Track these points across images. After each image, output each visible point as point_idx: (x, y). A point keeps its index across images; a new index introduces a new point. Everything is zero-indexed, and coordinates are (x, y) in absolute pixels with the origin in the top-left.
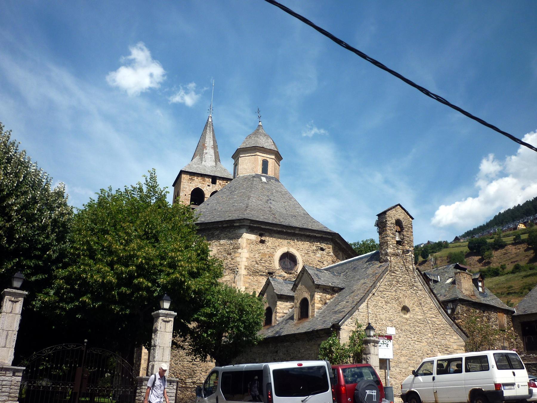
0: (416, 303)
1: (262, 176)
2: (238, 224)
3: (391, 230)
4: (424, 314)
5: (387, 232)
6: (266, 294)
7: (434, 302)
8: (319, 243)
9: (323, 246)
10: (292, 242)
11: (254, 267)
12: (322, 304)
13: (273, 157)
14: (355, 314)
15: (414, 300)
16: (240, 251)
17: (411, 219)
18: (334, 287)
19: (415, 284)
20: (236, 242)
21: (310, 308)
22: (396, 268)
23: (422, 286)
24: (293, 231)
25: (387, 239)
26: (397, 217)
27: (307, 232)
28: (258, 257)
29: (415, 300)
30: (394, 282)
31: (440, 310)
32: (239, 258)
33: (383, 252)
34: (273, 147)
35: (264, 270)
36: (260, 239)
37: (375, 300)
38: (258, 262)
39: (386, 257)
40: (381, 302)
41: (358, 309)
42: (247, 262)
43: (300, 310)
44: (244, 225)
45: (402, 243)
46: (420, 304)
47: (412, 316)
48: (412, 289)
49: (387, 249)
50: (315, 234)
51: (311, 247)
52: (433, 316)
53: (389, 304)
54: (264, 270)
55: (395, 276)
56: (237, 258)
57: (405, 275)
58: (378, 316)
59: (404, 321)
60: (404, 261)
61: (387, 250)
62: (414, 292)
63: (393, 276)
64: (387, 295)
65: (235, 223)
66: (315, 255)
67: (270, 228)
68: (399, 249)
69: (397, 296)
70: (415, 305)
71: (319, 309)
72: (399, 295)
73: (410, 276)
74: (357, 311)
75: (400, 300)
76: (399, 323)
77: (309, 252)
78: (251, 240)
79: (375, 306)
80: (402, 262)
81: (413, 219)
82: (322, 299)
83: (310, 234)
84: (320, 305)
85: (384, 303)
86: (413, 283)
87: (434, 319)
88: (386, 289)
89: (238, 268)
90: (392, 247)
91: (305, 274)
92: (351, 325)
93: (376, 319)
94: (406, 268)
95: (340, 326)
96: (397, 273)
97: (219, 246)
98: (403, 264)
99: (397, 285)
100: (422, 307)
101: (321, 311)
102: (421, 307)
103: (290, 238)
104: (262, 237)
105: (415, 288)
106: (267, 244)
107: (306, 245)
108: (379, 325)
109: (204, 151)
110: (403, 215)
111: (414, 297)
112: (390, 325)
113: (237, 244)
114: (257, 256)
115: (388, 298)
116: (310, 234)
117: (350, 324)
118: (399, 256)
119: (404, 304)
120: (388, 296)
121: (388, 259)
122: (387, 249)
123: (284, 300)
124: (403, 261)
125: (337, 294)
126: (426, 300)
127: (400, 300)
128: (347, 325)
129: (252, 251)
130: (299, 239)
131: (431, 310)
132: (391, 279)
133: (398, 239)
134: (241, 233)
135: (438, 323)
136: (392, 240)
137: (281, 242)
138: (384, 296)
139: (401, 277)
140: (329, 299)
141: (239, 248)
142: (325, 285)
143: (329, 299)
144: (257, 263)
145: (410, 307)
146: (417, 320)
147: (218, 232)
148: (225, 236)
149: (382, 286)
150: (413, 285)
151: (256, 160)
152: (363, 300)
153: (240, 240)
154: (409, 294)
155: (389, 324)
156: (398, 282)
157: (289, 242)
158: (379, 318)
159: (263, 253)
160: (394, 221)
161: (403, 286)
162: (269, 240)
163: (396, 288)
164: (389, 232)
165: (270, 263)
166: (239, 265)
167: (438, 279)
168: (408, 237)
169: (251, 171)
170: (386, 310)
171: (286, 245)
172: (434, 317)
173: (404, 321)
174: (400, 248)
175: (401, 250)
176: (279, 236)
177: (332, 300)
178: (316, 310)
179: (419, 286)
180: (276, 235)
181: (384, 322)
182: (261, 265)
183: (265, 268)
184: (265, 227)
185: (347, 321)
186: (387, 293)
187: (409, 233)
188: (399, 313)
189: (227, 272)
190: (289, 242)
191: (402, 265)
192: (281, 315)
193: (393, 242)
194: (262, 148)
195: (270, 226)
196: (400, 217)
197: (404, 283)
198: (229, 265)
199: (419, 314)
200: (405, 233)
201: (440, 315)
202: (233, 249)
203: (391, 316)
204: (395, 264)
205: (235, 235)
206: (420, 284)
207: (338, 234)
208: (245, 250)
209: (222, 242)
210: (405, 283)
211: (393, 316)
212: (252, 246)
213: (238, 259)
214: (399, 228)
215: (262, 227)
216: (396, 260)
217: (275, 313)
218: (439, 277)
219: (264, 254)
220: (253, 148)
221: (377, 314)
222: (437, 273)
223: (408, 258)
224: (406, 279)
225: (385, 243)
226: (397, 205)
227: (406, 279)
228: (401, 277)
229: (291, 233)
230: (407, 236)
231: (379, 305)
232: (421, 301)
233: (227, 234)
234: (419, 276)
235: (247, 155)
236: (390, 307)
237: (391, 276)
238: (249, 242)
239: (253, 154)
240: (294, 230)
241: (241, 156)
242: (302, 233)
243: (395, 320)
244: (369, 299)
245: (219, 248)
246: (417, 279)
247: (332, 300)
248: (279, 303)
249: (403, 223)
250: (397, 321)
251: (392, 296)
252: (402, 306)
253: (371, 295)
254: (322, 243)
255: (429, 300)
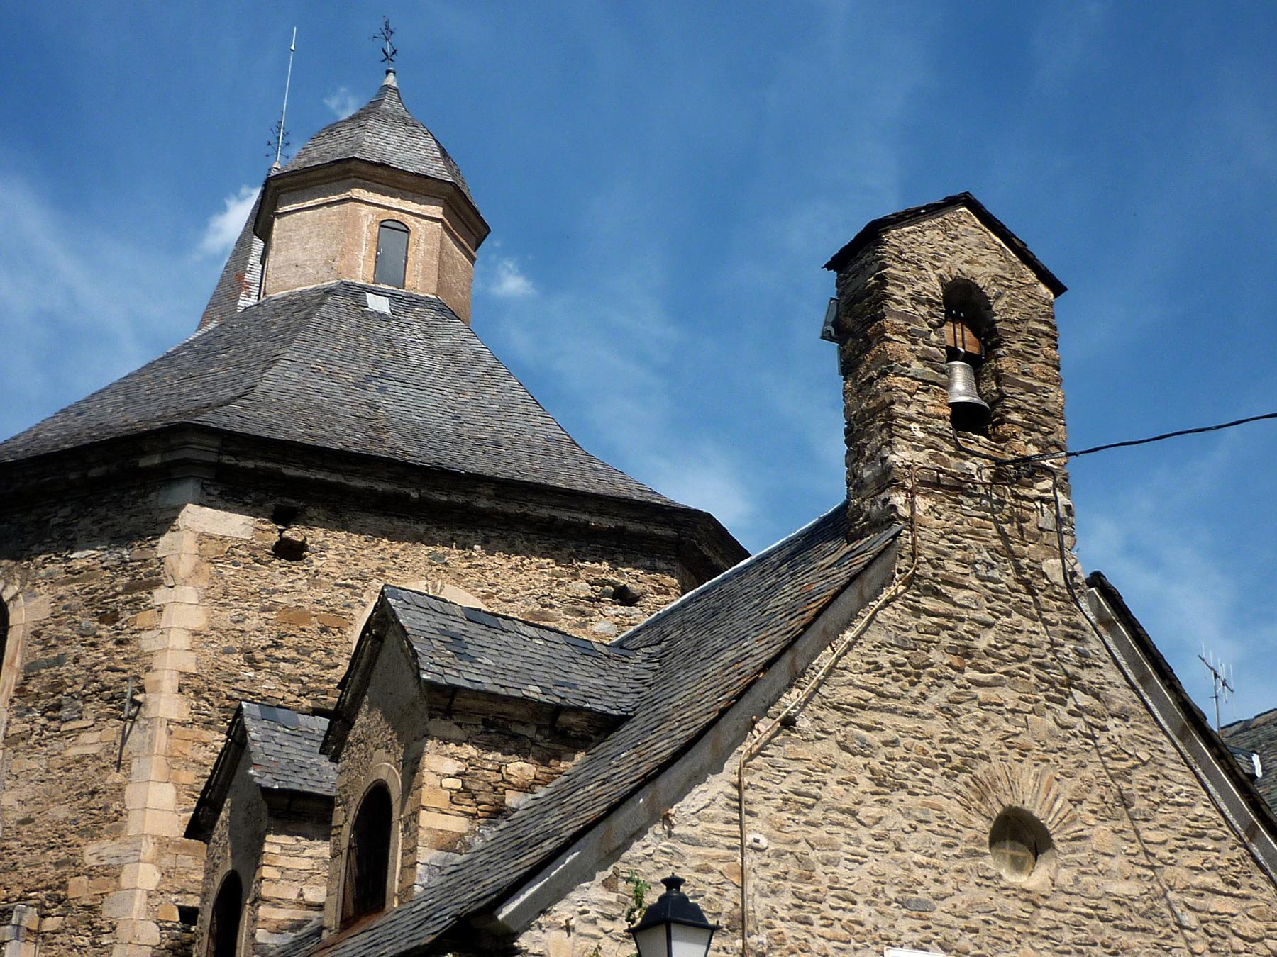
0: (1093, 797)
1: (375, 292)
2: (156, 460)
3: (913, 337)
4: (1152, 868)
5: (890, 346)
6: (228, 803)
7: (1218, 797)
8: (605, 566)
9: (630, 577)
10: (455, 557)
11: (234, 678)
12: (474, 816)
13: (436, 211)
14: (636, 850)
15: (1082, 773)
16: (159, 595)
17: (1043, 290)
18: (558, 710)
19: (1086, 675)
20: (148, 554)
21: (398, 840)
22: (950, 565)
23: (1133, 688)
24: (458, 498)
25: (889, 389)
26: (955, 265)
27: (541, 505)
28: (261, 631)
29: (1087, 774)
30: (935, 656)
31: (1255, 848)
32: (156, 633)
33: (867, 474)
34: (436, 169)
35: (291, 698)
36: (275, 537)
37: (801, 766)
38: (259, 655)
39: (882, 496)
40: (839, 775)
41: (666, 819)
42: (192, 655)
43: (354, 865)
44: (186, 463)
45: (996, 425)
46: (1124, 800)
47: (1065, 877)
48: (1063, 703)
49: (889, 444)
50: (584, 517)
51: (559, 583)
52: (1211, 880)
53: (902, 794)
54: (291, 698)
55: (945, 616)
56: (144, 635)
57: (1016, 617)
58: (819, 869)
59: (1014, 907)
60: (1007, 527)
61: (886, 451)
62: (1080, 724)
63: (930, 614)
64: (890, 734)
65: (144, 454)
66: (584, 625)
67: (334, 478)
68: (974, 454)
69: (955, 746)
70: (1086, 806)
71: (450, 844)
72: (971, 739)
73: (1046, 623)
74: (658, 828)
75: (978, 773)
76: (976, 920)
77: (551, 606)
78: (222, 540)
79: (799, 801)
80: (994, 531)
81: (1058, 288)
82: (474, 786)
83: (555, 513)
84: (458, 824)
85: (865, 784)
86: (1069, 669)
87: (1217, 904)
88: (880, 695)
89: (142, 690)
90: (920, 434)
91: (391, 640)
92: (608, 925)
93: (807, 889)
94: (1019, 570)
95: (515, 935)
96: (959, 596)
97: (62, 584)
98: (996, 543)
99: (961, 671)
100: (1133, 819)
101: (459, 859)
102: (1125, 823)
103: (447, 535)
104: (288, 527)
105: (1082, 699)
106: (316, 563)
107: (533, 575)
108: (827, 932)
109: (241, 303)
110: (995, 258)
111: (1081, 757)
112: (909, 937)
113: (151, 565)
114: (253, 622)
115: (898, 752)
116: (555, 513)
117: (594, 922)
118: (971, 496)
119: (1007, 801)
120: (894, 743)
121: (894, 507)
122: (889, 444)
123: (308, 828)
124: (1001, 531)
125: (580, 757)
126: (1161, 782)
127: (981, 769)
128: (568, 929)
129: (225, 595)
130: (494, 542)
131: (1199, 843)
132: (914, 634)
133: (961, 388)
134: (174, 503)
135: (1249, 927)
136: (922, 396)
137: (395, 556)
138: (863, 740)
139: (989, 625)
140: (526, 788)
141: (158, 584)
142: (494, 696)
143: (526, 788)
144: (252, 662)
145: (1050, 822)
146: (1103, 903)
147: (66, 511)
148: (95, 528)
149: (849, 676)
150: (1071, 681)
151: (355, 220)
152: (703, 753)
153: (165, 540)
154: (1043, 735)
155: (903, 925)
156: (969, 656)
157: (439, 558)
158: (822, 888)
159: (287, 608)
160: (934, 288)
161: (997, 683)
162: (330, 542)
163: (950, 689)
164: (899, 346)
165: (328, 662)
166: (148, 669)
167: (1253, 768)
168: (1031, 389)
169: (324, 272)
170: (877, 830)
171: (421, 571)
172: (1221, 886)
173: (1014, 907)
174: (975, 448)
175: (981, 462)
176: (385, 523)
177: (541, 792)
178: (426, 855)
179: (1112, 691)
180: (371, 520)
181: (863, 911)
182: (273, 671)
183: (294, 687)
184: (301, 473)
185: (573, 896)
186: (887, 719)
187: (1035, 368)
188: (975, 854)
189: (92, 709)
190: (439, 558)
191: (990, 550)
192: (282, 915)
193: (931, 410)
194: (380, 171)
195: (333, 470)
196: (977, 270)
197: (1006, 662)
198: (102, 676)
199: (1114, 864)
200: (1008, 365)
201: (1258, 878)
202: (128, 589)
203: (918, 874)
204: (944, 543)
205: (142, 519)
206: (1119, 679)
207: (708, 516)
208: (189, 594)
209: (81, 558)
210: (1014, 667)
211: (932, 874)
212: (229, 571)
213: (148, 641)
214: (968, 334)
215: (290, 472)
216: (950, 517)
217: (251, 904)
218: (1256, 758)
219: (297, 616)
220: (336, 168)
221: (814, 855)
222: (1248, 744)
223: (1033, 516)
224: (1023, 639)
225: (873, 412)
226: (952, 202)
227: (1023, 639)
228: (989, 625)
229: (451, 506)
230: (1023, 385)
231: (826, 795)
232: (1125, 785)
233: (106, 518)
234: (1108, 624)
235: (307, 204)
236: (907, 814)
237: (917, 612)
238: (212, 549)
239: (337, 198)
240: (466, 493)
241: (281, 210)
242: (513, 508)
243: (949, 901)
244: (752, 757)
245: (62, 591)
246: (1094, 645)
247: (541, 792)
248: (274, 844)
249: (998, 306)
250: (961, 907)
251: (924, 744)
252: (999, 810)
253: (764, 726)
254: (626, 563)
255: (1180, 780)
